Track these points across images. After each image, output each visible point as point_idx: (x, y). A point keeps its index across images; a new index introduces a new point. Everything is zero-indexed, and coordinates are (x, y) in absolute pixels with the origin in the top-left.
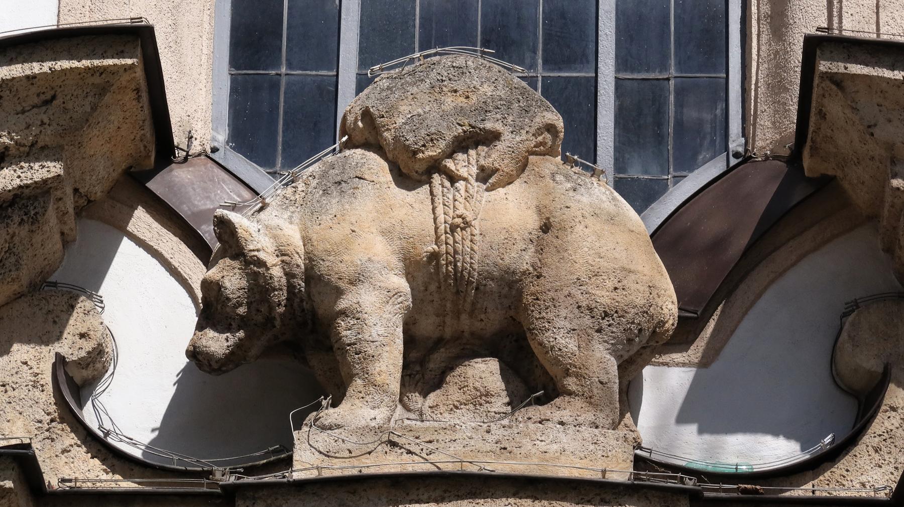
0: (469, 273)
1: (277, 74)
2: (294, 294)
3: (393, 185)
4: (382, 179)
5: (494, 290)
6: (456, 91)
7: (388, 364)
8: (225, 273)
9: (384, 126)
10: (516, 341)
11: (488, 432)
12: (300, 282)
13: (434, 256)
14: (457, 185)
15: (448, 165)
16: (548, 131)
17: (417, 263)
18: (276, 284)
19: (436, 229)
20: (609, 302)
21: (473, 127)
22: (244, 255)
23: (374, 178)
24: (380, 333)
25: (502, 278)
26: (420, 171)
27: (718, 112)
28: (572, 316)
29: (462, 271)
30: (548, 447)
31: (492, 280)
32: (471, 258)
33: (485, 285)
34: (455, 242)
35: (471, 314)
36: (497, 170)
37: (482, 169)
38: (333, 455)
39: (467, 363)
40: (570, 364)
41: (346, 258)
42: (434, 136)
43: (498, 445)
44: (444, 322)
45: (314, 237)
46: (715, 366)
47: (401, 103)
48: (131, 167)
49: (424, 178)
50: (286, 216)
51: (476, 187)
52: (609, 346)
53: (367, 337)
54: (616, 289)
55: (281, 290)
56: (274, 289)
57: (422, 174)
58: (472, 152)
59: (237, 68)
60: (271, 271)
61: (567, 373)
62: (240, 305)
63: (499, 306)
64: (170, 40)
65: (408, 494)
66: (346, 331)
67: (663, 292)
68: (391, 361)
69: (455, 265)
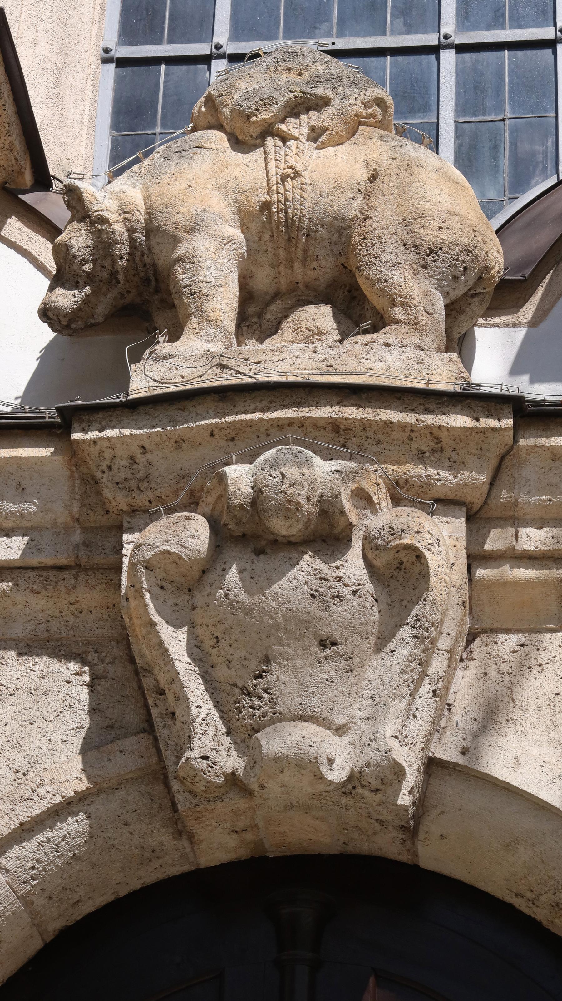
0: (300, 219)
1: (153, 134)
2: (135, 248)
3: (230, 150)
4: (219, 146)
5: (324, 236)
6: (289, 69)
7: (223, 303)
8: (72, 235)
9: (223, 103)
10: (349, 291)
11: (315, 352)
12: (141, 236)
13: (266, 206)
14: (288, 143)
15: (280, 127)
16: (379, 106)
17: (251, 213)
18: (118, 238)
19: (268, 180)
20: (433, 239)
21: (304, 93)
22: (89, 217)
23: (213, 146)
24: (215, 275)
25: (332, 225)
26: (255, 135)
27: (549, 144)
28: (398, 251)
29: (293, 217)
30: (373, 365)
31: (323, 226)
32: (301, 205)
33: (316, 231)
34: (286, 190)
35: (304, 263)
36: (327, 129)
37: (313, 129)
38: (167, 381)
39: (301, 309)
40: (396, 294)
41: (183, 209)
42: (267, 101)
43: (325, 363)
44: (279, 273)
45: (154, 194)
46: (543, 326)
47: (239, 81)
48: (6, 183)
49: (258, 141)
50: (129, 183)
51: (308, 146)
52: (435, 281)
53: (201, 278)
54: (440, 228)
55: (123, 244)
56: (117, 243)
57: (257, 138)
58: (303, 117)
59: (117, 131)
60: (113, 227)
61: (393, 303)
62: (86, 262)
63: (330, 253)
64: (51, 93)
65: (234, 406)
66: (182, 276)
67: (488, 240)
68: (225, 301)
69: (286, 213)
